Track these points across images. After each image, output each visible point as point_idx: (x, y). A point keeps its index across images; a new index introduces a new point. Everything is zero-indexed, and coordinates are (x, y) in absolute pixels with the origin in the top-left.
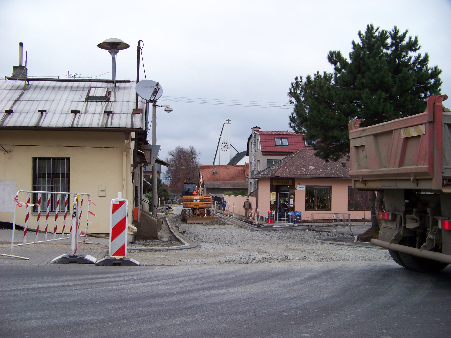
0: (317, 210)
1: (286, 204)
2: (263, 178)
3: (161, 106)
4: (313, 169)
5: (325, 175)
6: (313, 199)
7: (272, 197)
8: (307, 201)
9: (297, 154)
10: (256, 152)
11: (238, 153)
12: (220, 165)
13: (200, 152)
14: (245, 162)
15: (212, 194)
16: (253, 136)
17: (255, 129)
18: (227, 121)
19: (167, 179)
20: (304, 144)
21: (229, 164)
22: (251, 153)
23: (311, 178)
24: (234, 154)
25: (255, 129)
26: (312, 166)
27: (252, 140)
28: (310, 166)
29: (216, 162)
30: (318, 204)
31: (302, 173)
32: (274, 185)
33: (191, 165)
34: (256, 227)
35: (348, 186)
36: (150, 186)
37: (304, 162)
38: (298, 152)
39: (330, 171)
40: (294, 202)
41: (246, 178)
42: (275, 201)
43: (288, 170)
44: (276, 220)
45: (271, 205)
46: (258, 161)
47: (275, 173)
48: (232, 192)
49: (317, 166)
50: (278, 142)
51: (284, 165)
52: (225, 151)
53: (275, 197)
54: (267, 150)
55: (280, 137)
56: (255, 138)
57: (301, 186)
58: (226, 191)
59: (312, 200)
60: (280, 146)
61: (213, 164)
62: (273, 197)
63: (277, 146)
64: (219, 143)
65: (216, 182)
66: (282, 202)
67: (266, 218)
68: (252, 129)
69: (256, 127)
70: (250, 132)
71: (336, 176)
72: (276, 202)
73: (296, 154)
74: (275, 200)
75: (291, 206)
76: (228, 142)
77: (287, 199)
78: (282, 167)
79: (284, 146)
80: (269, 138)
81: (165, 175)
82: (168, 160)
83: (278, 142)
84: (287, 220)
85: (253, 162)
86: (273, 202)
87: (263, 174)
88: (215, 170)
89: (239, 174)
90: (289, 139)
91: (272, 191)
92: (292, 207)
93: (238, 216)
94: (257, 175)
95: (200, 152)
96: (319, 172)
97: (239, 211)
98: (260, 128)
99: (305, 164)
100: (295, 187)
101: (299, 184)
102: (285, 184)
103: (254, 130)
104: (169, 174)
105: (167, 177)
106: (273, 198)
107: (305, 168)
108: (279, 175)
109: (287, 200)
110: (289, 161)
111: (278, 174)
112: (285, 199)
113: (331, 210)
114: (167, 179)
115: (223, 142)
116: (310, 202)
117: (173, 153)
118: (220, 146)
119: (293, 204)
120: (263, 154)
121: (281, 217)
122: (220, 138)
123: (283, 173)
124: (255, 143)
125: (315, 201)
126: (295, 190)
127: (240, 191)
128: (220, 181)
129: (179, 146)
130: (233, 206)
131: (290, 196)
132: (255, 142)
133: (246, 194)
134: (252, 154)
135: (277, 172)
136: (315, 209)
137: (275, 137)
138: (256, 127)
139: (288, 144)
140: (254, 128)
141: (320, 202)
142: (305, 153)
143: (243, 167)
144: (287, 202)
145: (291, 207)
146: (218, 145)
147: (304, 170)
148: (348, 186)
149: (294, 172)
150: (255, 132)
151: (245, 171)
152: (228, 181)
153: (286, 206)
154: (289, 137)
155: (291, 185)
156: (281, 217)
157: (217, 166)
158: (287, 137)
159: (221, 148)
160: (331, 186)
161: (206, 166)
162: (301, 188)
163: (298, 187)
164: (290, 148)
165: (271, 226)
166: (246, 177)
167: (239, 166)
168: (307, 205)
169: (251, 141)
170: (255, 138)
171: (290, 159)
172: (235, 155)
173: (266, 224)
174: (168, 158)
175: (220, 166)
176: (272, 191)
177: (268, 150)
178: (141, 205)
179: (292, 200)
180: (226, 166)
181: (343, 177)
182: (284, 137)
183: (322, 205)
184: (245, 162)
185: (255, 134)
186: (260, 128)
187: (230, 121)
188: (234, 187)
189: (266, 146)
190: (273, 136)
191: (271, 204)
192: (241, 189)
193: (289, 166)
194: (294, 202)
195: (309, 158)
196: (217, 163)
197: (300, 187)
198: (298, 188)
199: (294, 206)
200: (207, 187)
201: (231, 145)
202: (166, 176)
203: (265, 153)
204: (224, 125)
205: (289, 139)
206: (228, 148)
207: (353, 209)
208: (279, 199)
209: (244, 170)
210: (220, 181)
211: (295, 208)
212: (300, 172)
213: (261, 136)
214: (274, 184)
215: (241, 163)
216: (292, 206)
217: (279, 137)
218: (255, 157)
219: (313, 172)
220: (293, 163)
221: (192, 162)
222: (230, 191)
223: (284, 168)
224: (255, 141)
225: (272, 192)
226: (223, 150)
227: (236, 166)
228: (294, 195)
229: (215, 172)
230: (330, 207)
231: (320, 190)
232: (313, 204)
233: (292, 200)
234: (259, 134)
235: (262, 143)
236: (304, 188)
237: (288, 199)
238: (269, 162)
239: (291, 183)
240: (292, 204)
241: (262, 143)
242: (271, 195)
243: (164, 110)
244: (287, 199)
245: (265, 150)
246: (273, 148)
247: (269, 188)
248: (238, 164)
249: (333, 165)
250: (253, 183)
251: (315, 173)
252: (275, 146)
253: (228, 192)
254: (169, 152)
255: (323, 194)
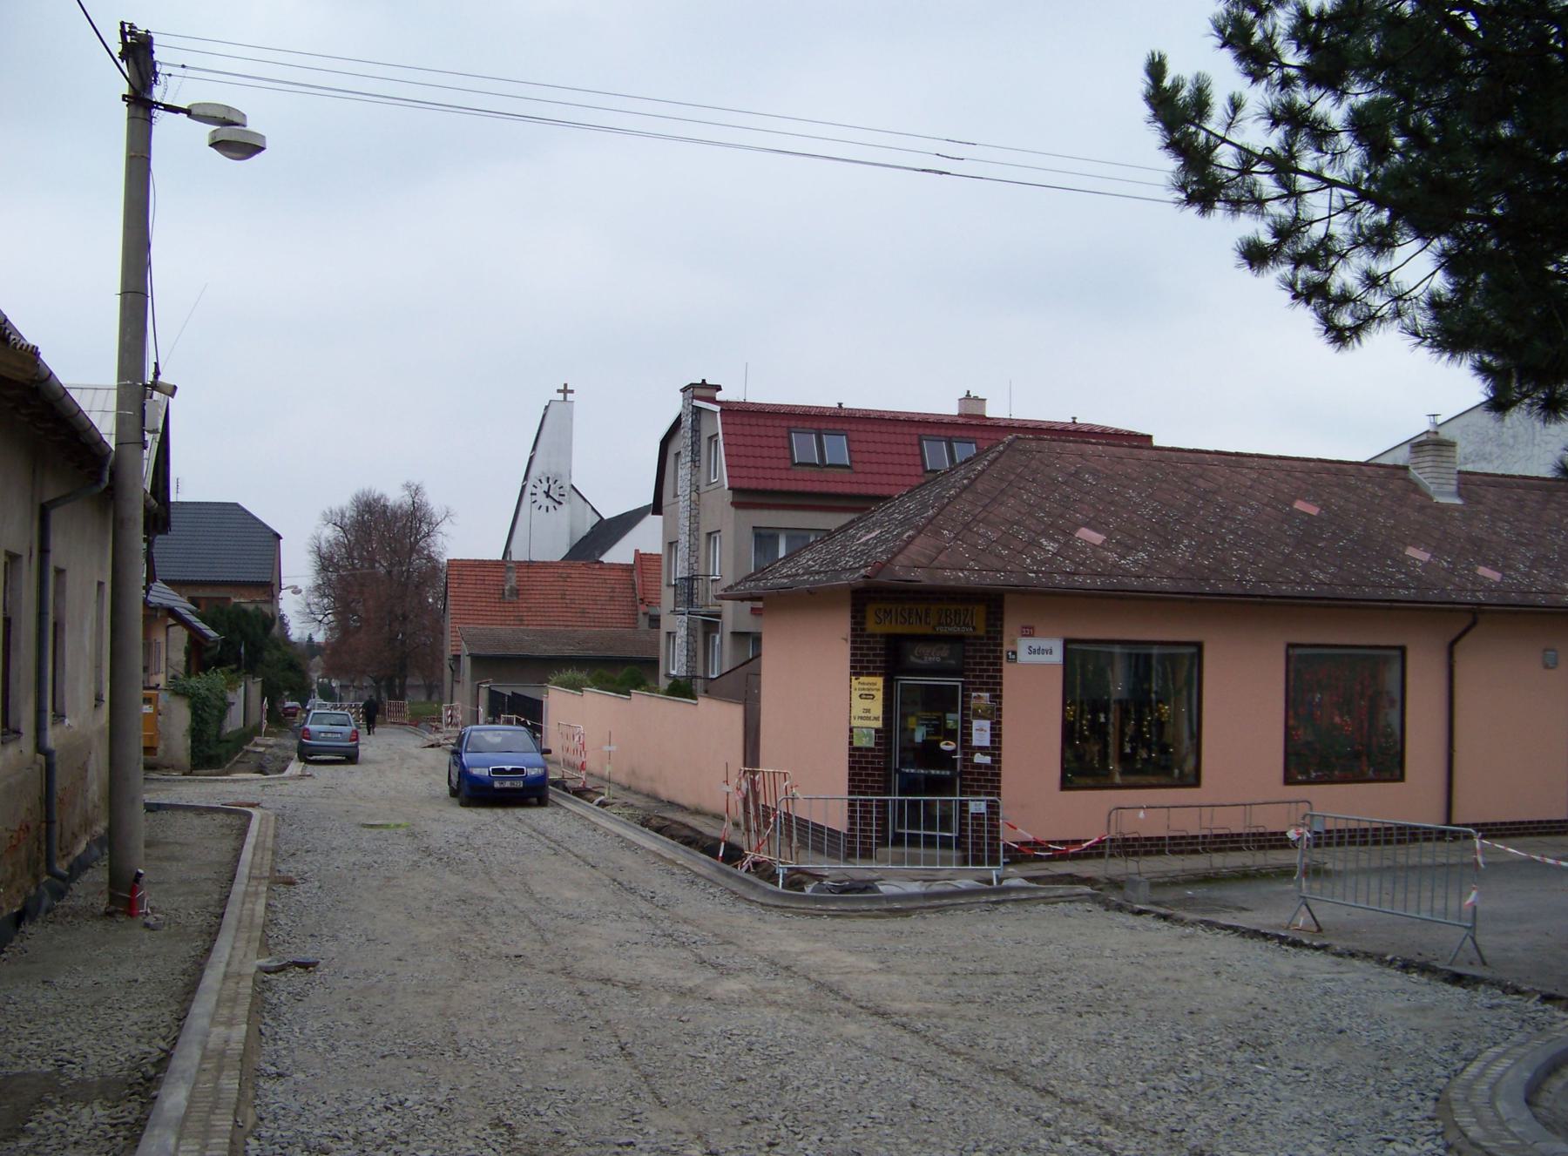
0: (1118, 779)
1: (943, 746)
2: (809, 591)
3: (188, 112)
4: (1101, 546)
5: (1170, 577)
6: (1102, 719)
7: (859, 706)
8: (1069, 732)
9: (996, 459)
10: (701, 496)
11: (602, 518)
12: (531, 561)
13: (447, 508)
14: (637, 551)
15: (494, 682)
16: (687, 422)
17: (699, 392)
18: (559, 391)
19: (315, 620)
20: (918, 460)
21: (563, 559)
22: (679, 505)
23: (1101, 597)
24: (587, 524)
25: (699, 392)
26: (1087, 525)
27: (682, 442)
28: (1077, 526)
29: (513, 547)
30: (1128, 750)
31: (1043, 563)
32: (873, 636)
33: (410, 563)
34: (777, 894)
35: (1290, 646)
36: (210, 645)
37: (1042, 509)
38: (1001, 453)
39: (1194, 556)
40: (996, 734)
41: (641, 616)
42: (877, 731)
43: (962, 547)
44: (883, 842)
45: (858, 759)
46: (709, 534)
47: (889, 561)
48: (588, 675)
49: (1116, 529)
50: (804, 447)
51: (934, 517)
52: (551, 508)
53: (877, 708)
54: (753, 485)
55: (815, 425)
56: (696, 430)
57: (1035, 643)
58: (560, 671)
59: (1094, 724)
60: (814, 465)
61: (500, 558)
62: (867, 703)
63: (799, 464)
64: (526, 478)
65: (513, 631)
66: (919, 737)
67: (833, 833)
68: (684, 390)
69: (704, 380)
70: (673, 406)
71: (1232, 588)
72: (884, 735)
73: (992, 463)
74: (879, 724)
75: (979, 758)
76: (561, 476)
77: (949, 716)
78: (925, 526)
79: (830, 466)
80: (756, 431)
81: (309, 605)
82: (323, 543)
83: (804, 447)
84: (946, 843)
85: (684, 539)
86: (869, 735)
87: (797, 575)
88: (512, 580)
89: (612, 599)
90: (855, 436)
91: (858, 668)
92: (987, 766)
93: (639, 801)
94: (759, 580)
95: (447, 508)
96: (1135, 562)
97: (633, 773)
98: (718, 388)
99: (1048, 514)
100: (1006, 647)
101: (1029, 632)
102: (942, 630)
103: (694, 397)
104: (326, 601)
105: (317, 611)
106: (868, 711)
107: (1057, 541)
108: (921, 577)
109: (950, 724)
110: (958, 495)
111: (912, 569)
112: (943, 720)
113: (1196, 782)
114: (315, 620)
115: (543, 473)
116: (1084, 739)
117: (343, 516)
118: (529, 489)
119: (995, 749)
120: (736, 500)
121: (914, 824)
122: (531, 459)
123: (936, 563)
124: (695, 453)
125: (1111, 729)
126: (1006, 666)
127: (625, 670)
128: (530, 627)
129: (367, 489)
130: (606, 748)
131: (973, 703)
132: (696, 448)
133: (651, 684)
134: (683, 503)
135: (900, 557)
136: (1109, 774)
137: (788, 427)
138: (704, 380)
139: (851, 461)
140: (693, 386)
141: (1138, 738)
142: (1038, 455)
143: (627, 568)
144: (951, 735)
145: (979, 766)
146: (523, 488)
147: (1051, 547)
148: (1290, 646)
149: (1001, 557)
150: (698, 403)
151: (634, 589)
152: (562, 628)
153: (946, 760)
154: (854, 427)
155: (981, 638)
156: (914, 824)
157: (520, 564)
158: (846, 426)
159: (534, 498)
160: (1199, 646)
161: (471, 566)
162: (1039, 651)
163: (1023, 645)
164: (861, 478)
165: (866, 887)
166: (641, 612)
167: (613, 567)
168: (1069, 755)
169: (673, 449)
170: (696, 430)
171: (966, 488)
172: (588, 529)
173: (831, 868)
174: (323, 537)
175: (529, 564)
176: (858, 668)
177: (762, 485)
178: (41, 758)
179: (986, 724)
180: (558, 567)
181: (1271, 592)
182: (831, 426)
183: (1150, 752)
184: (637, 551)
185: (697, 411)
186: (718, 388)
187: (572, 391)
188: (591, 653)
189: (744, 474)
190: (785, 423)
191: (856, 743)
192: (624, 661)
193: (966, 525)
194: (996, 734)
195: (1065, 483)
196: (518, 555)
197: (1032, 651)
198: (1023, 656)
199: (997, 760)
200: (476, 651)
201: (573, 486)
202: (314, 608)
203: (745, 497)
204: (547, 407)
205: (855, 436)
206: (557, 505)
207: (1309, 777)
208: (904, 717)
209: (634, 584)
210: (530, 627)
211: (1003, 772)
212: (1033, 557)
213: (730, 420)
214: (872, 626)
215: (620, 553)
216: (987, 760)
217: (808, 424)
218: (694, 518)
219: (1104, 560)
220: (985, 507)
221: (413, 548)
222: (581, 671)
223: (937, 533)
224: (695, 443)
225: (862, 679)
226: (544, 509)
227: (597, 566)
228: (997, 697)
229: (512, 589)
230: (1189, 765)
231: (1141, 660)
232: (1096, 748)
233: (986, 724)
234: (717, 408)
235: (734, 450)
236: (1057, 657)
237: (958, 716)
238: (765, 539)
239: (977, 623)
240: (982, 750)
241: (734, 450)
242: (855, 695)
243: (206, 140)
244: (953, 720)
245: (745, 484)
246: (784, 474)
247: (841, 654)
248: (609, 557)
249: (1199, 528)
250: (682, 633)
251: (1115, 565)
252: (789, 465)
253: (568, 675)
254: (325, 514)
255: (1154, 688)
